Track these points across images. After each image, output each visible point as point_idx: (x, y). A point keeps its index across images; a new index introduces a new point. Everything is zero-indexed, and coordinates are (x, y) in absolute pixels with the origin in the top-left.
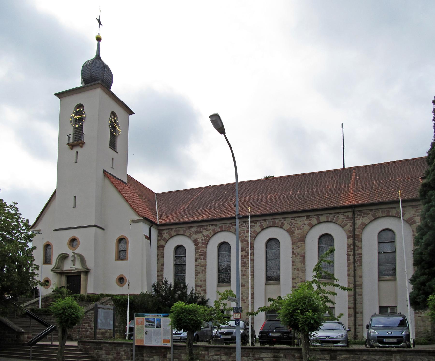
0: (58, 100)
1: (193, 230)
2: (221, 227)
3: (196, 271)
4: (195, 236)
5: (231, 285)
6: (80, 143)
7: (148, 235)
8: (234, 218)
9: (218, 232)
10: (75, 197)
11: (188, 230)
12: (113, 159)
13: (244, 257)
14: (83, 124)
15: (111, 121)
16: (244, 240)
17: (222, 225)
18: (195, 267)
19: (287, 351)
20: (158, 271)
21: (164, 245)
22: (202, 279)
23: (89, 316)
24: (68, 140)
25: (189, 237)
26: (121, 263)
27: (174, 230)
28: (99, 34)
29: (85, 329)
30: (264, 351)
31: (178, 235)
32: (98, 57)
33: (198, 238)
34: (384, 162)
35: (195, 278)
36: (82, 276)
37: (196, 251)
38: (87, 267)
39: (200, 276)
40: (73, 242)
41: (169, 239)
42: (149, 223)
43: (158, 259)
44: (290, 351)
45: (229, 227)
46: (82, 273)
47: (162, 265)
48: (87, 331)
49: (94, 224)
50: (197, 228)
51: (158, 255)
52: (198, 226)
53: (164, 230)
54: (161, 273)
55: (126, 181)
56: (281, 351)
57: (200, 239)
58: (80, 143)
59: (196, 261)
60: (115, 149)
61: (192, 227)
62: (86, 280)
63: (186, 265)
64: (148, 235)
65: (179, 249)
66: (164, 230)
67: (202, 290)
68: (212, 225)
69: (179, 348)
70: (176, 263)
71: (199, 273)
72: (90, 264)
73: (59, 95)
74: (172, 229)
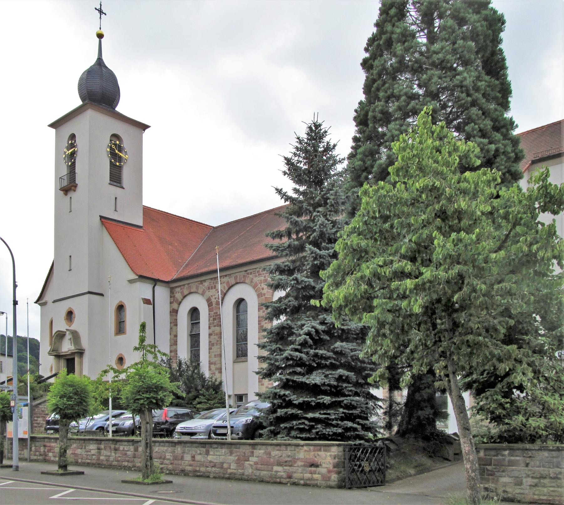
0: (53, 131)
1: (206, 284)
2: (236, 278)
3: (210, 342)
4: (208, 294)
5: (249, 360)
6: (72, 186)
7: (150, 298)
8: (215, 271)
9: (232, 286)
10: (70, 256)
11: (201, 285)
12: (116, 198)
13: (261, 319)
14: (75, 160)
15: (111, 147)
16: (261, 293)
17: (237, 274)
18: (209, 337)
19: (106, 442)
20: (171, 346)
21: (176, 309)
22: (216, 353)
23: (43, 409)
24: (61, 183)
25: (203, 294)
26: (121, 337)
27: (186, 286)
28: (100, 28)
29: (38, 424)
30: (91, 442)
31: (190, 293)
32: (100, 62)
33: (212, 296)
34: (546, 124)
35: (209, 353)
36: (77, 360)
37: (209, 314)
38: (81, 346)
39: (215, 348)
40: (70, 314)
41: (182, 300)
42: (152, 282)
43: (171, 328)
44: (108, 442)
45: (244, 276)
46: (76, 355)
47: (176, 336)
48: (41, 426)
49: (86, 291)
50: (210, 281)
51: (171, 323)
52: (211, 279)
53: (176, 287)
54: (174, 347)
55: (141, 224)
56: (103, 442)
57: (214, 297)
58: (72, 186)
59: (209, 328)
60: (120, 183)
61: (205, 281)
62: (81, 364)
63: (201, 335)
64: (150, 298)
65: (194, 312)
66: (176, 287)
67: (216, 369)
68: (226, 276)
69: (39, 440)
70: (191, 332)
71: (213, 345)
72: (85, 343)
73: (53, 125)
74: (184, 285)
